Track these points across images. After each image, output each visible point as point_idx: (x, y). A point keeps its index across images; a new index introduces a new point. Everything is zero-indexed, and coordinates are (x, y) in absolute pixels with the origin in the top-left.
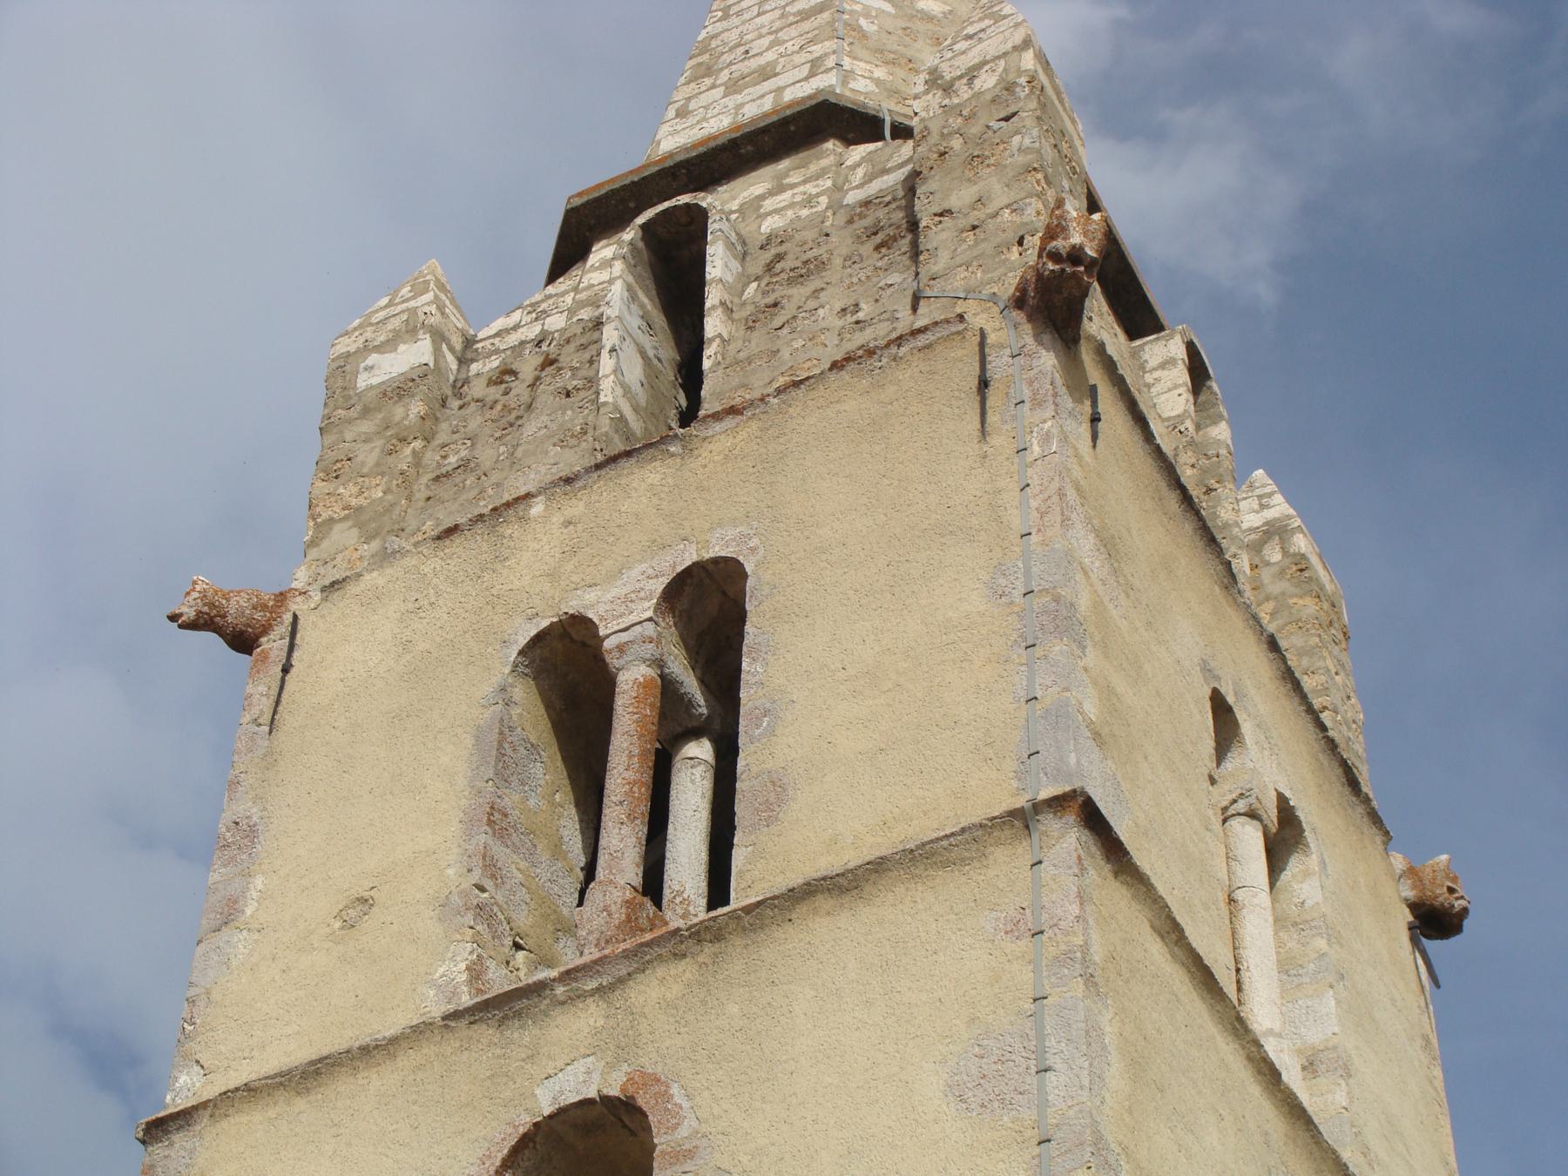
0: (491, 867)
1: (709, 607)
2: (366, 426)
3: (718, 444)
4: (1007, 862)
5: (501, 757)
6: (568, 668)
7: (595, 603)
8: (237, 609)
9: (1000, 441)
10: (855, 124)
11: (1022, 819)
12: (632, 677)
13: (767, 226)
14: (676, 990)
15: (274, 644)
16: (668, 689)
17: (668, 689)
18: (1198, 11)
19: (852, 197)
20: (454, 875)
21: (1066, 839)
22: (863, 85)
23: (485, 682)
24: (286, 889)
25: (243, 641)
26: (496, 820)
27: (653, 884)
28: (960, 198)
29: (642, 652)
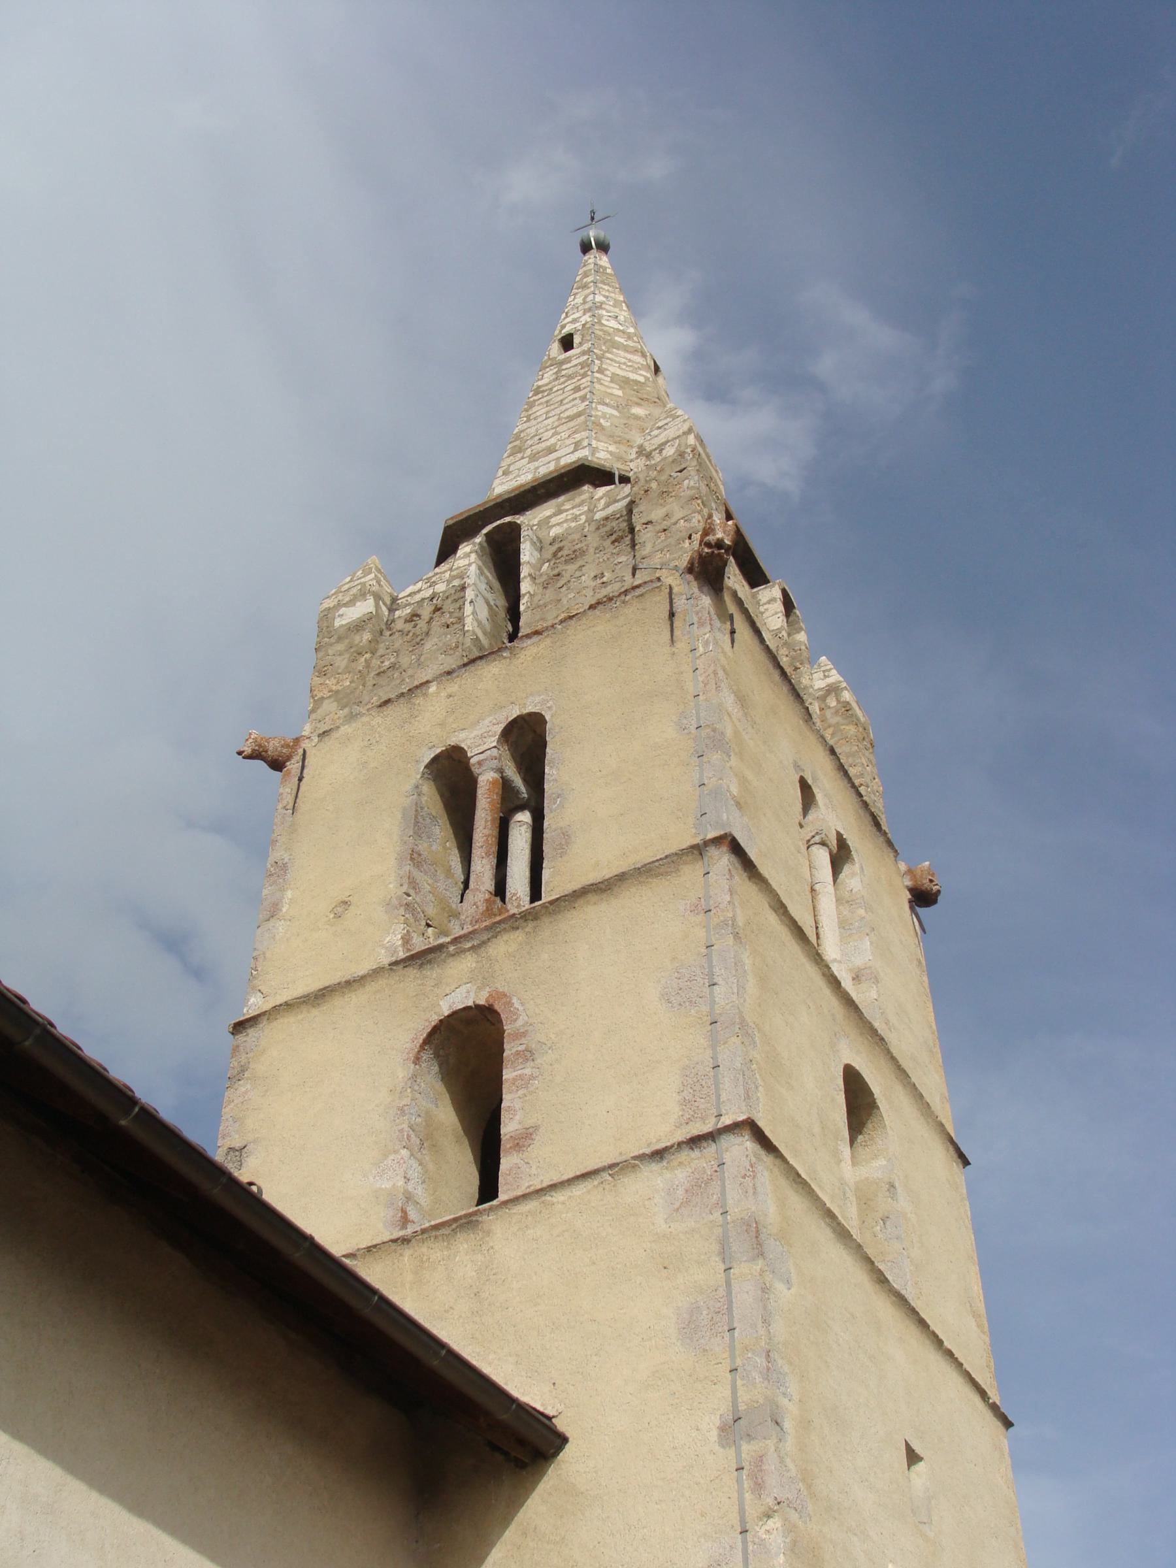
1: (527, 739)
2: (340, 647)
3: (529, 651)
4: (691, 873)
5: (417, 824)
6: (452, 775)
9: (682, 646)
11: (698, 850)
12: (486, 779)
15: (293, 766)
16: (506, 785)
19: (598, 516)
20: (393, 888)
22: (603, 455)
23: (408, 785)
24: (304, 896)
25: (277, 765)
27: (500, 889)
28: (657, 514)
29: (490, 764)
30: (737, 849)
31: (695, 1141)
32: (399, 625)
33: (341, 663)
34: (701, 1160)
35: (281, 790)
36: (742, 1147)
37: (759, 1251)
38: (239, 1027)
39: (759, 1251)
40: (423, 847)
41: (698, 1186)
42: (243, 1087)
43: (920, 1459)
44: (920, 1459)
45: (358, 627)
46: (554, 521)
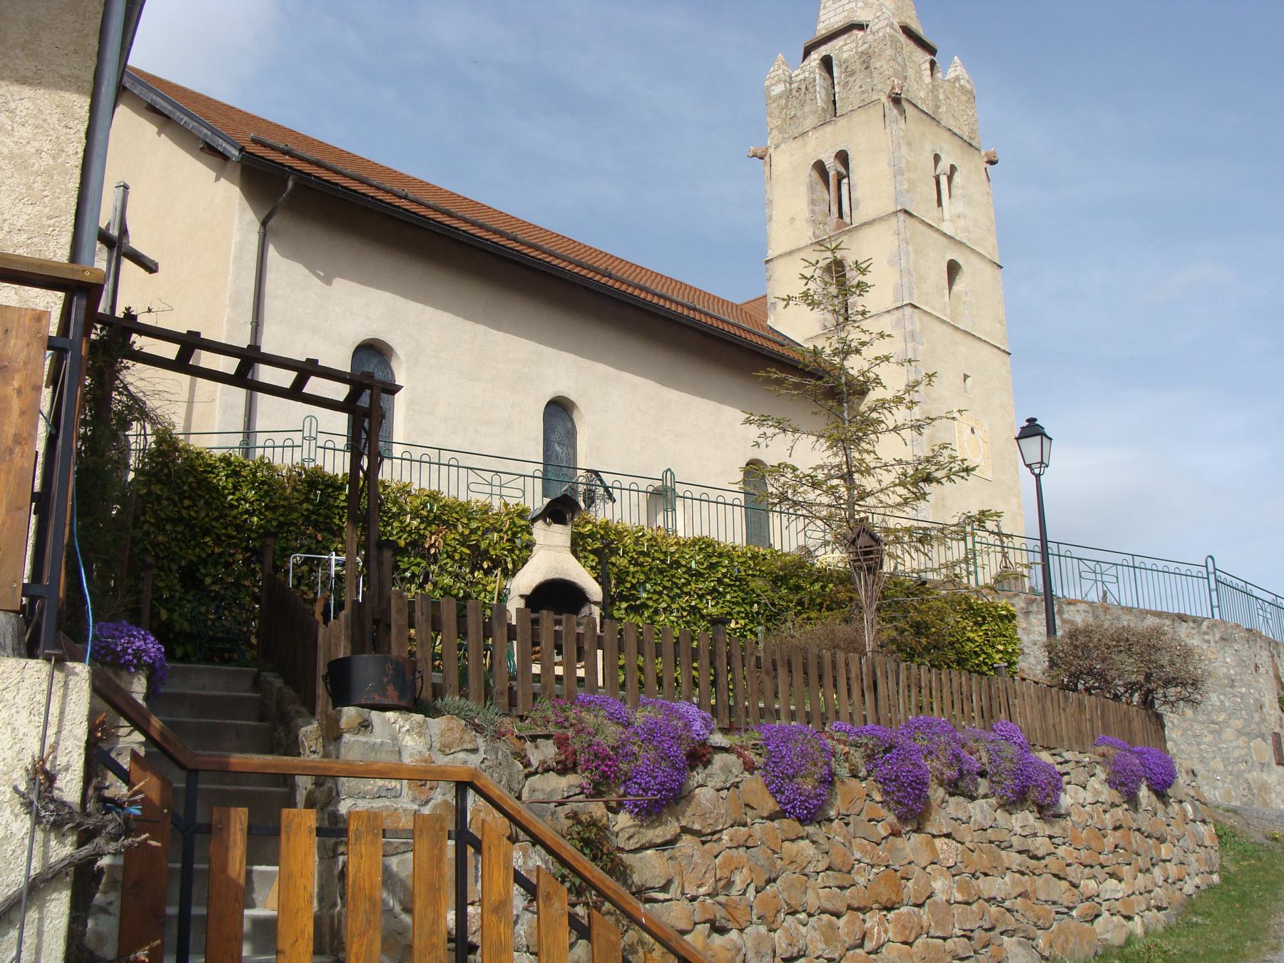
0: (813, 212)
1: (843, 157)
2: (775, 105)
3: (842, 122)
4: (894, 220)
5: (812, 189)
6: (820, 167)
7: (823, 157)
8: (759, 153)
9: (888, 130)
10: (861, 27)
11: (896, 213)
12: (832, 173)
13: (845, 55)
14: (112, 789)
15: (767, 158)
16: (839, 173)
17: (839, 173)
18: (512, 959)
19: (860, 50)
20: (807, 214)
21: (902, 216)
22: (861, 17)
23: (807, 173)
24: (780, 214)
25: (762, 158)
26: (813, 202)
27: (841, 216)
28: (878, 65)
29: (832, 166)
30: (906, 212)
31: (897, 308)
32: (794, 93)
33: (777, 112)
34: (899, 313)
35: (1033, 662)
36: (909, 310)
37: (913, 339)
38: (767, 262)
39: (913, 339)
40: (815, 197)
41: (898, 321)
42: (772, 282)
43: (1032, 421)
44: (1032, 421)
45: (780, 97)
46: (845, 48)
